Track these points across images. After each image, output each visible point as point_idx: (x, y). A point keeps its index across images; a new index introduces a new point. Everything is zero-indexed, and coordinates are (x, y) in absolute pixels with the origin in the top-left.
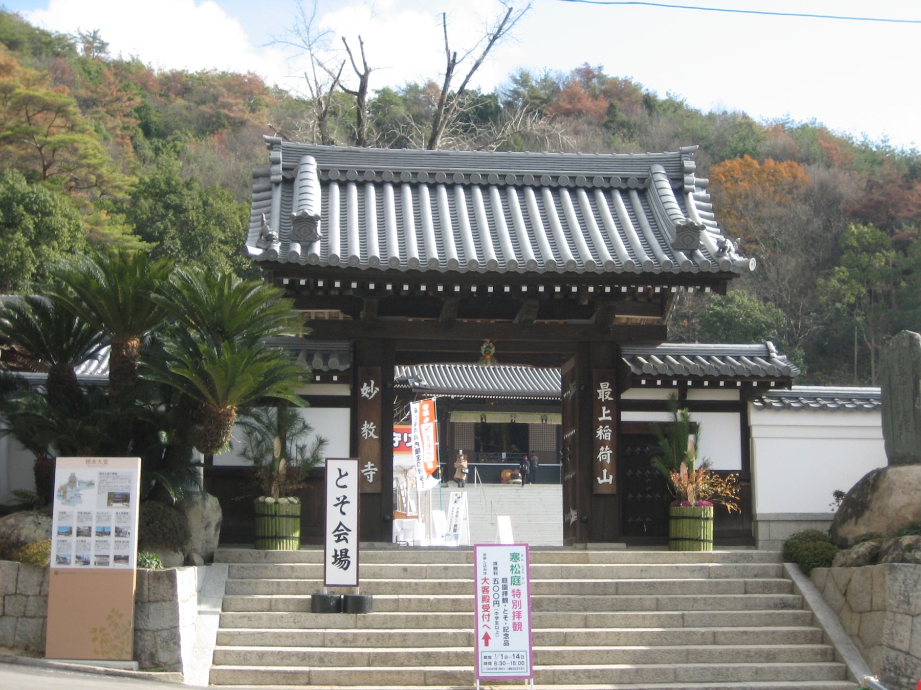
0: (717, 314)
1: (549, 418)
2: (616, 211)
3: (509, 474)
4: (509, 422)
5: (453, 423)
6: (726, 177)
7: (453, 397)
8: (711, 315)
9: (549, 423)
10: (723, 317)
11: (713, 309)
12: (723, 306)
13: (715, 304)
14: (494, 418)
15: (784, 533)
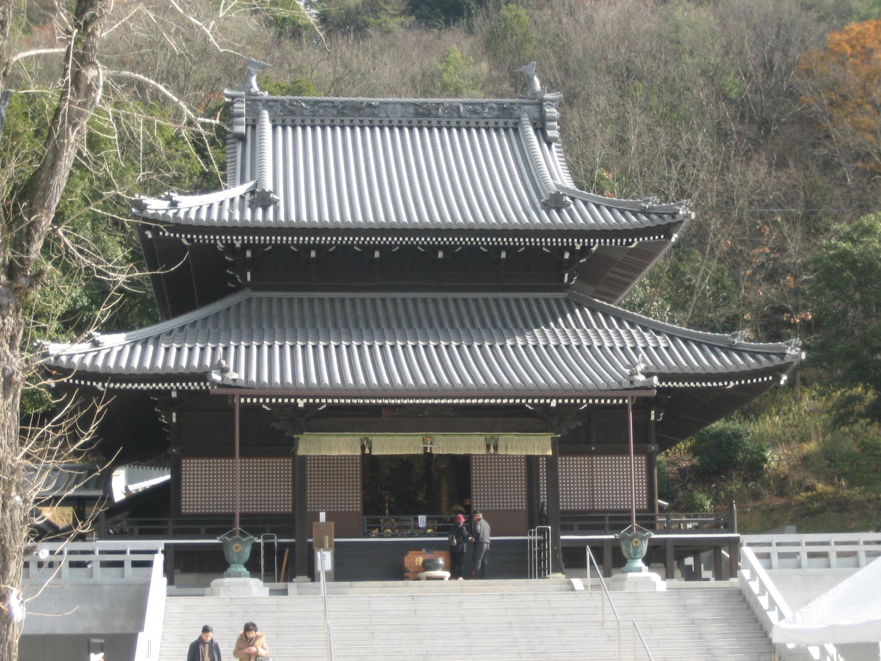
0: (843, 255)
1: (501, 444)
2: (488, 150)
3: (420, 560)
4: (420, 452)
5: (304, 458)
6: (853, 47)
7: (301, 403)
8: (832, 258)
9: (501, 452)
10: (855, 261)
11: (835, 247)
12: (854, 242)
13: (841, 239)
14: (389, 445)
15: (233, 569)
